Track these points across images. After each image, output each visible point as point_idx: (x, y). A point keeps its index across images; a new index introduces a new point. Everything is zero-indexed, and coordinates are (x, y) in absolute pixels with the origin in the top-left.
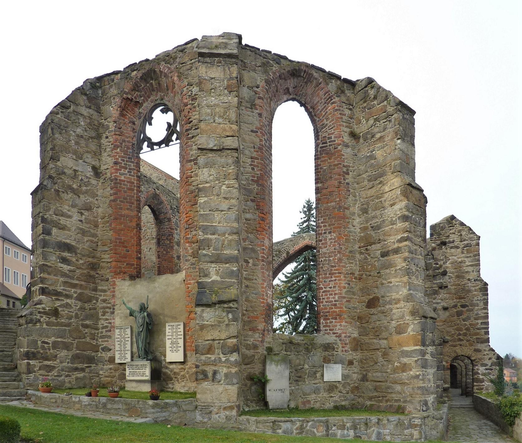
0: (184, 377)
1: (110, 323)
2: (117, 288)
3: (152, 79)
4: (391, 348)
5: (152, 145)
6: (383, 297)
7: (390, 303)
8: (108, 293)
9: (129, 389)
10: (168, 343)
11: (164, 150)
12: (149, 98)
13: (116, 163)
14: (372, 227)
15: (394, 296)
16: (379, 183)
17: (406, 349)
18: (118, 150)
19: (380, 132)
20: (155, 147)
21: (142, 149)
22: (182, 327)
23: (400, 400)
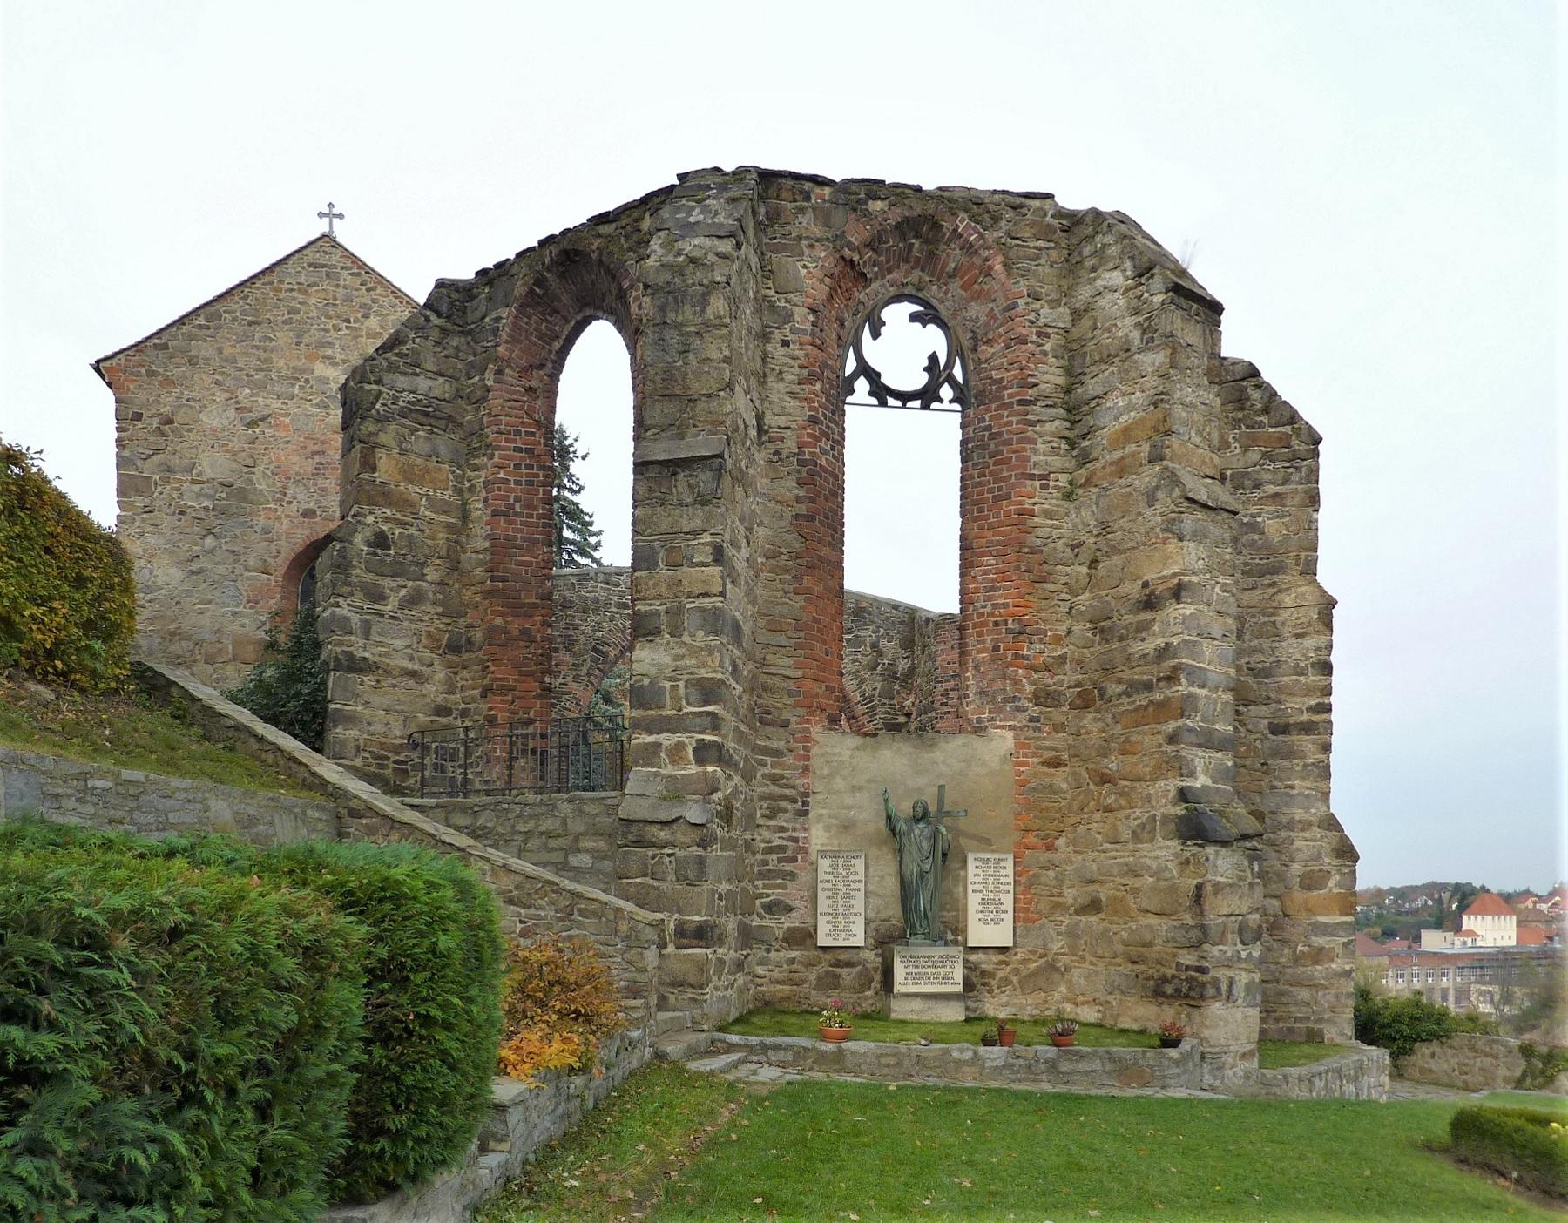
0: (1006, 981)
1: (796, 840)
2: (815, 750)
3: (917, 236)
4: (1286, 915)
5: (881, 393)
6: (1273, 813)
7: (1290, 826)
8: (789, 759)
9: (901, 1017)
10: (973, 902)
11: (913, 416)
12: (890, 272)
13: (813, 420)
14: (1251, 669)
15: (1299, 814)
16: (1271, 585)
17: (1322, 919)
18: (818, 386)
19: (1274, 483)
20: (891, 401)
21: (852, 392)
22: (1010, 864)
23: (1308, 1018)
